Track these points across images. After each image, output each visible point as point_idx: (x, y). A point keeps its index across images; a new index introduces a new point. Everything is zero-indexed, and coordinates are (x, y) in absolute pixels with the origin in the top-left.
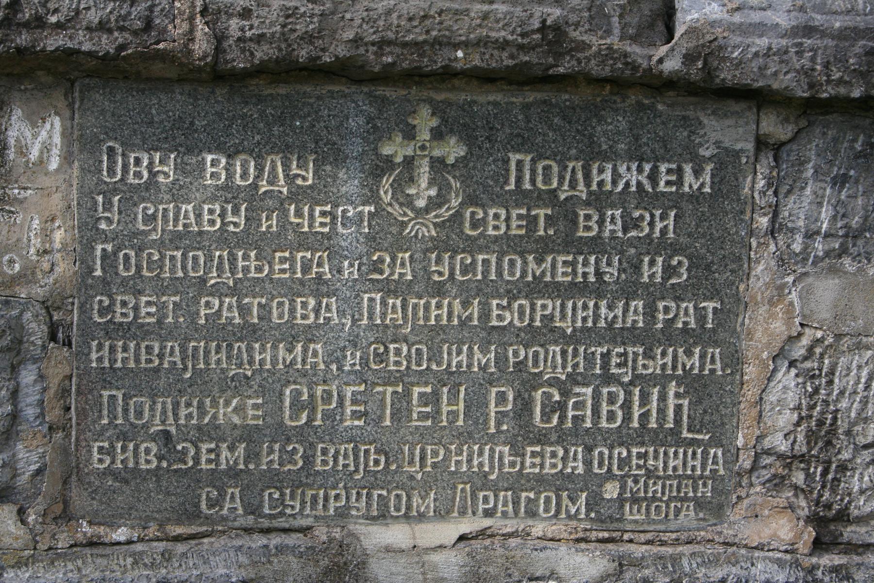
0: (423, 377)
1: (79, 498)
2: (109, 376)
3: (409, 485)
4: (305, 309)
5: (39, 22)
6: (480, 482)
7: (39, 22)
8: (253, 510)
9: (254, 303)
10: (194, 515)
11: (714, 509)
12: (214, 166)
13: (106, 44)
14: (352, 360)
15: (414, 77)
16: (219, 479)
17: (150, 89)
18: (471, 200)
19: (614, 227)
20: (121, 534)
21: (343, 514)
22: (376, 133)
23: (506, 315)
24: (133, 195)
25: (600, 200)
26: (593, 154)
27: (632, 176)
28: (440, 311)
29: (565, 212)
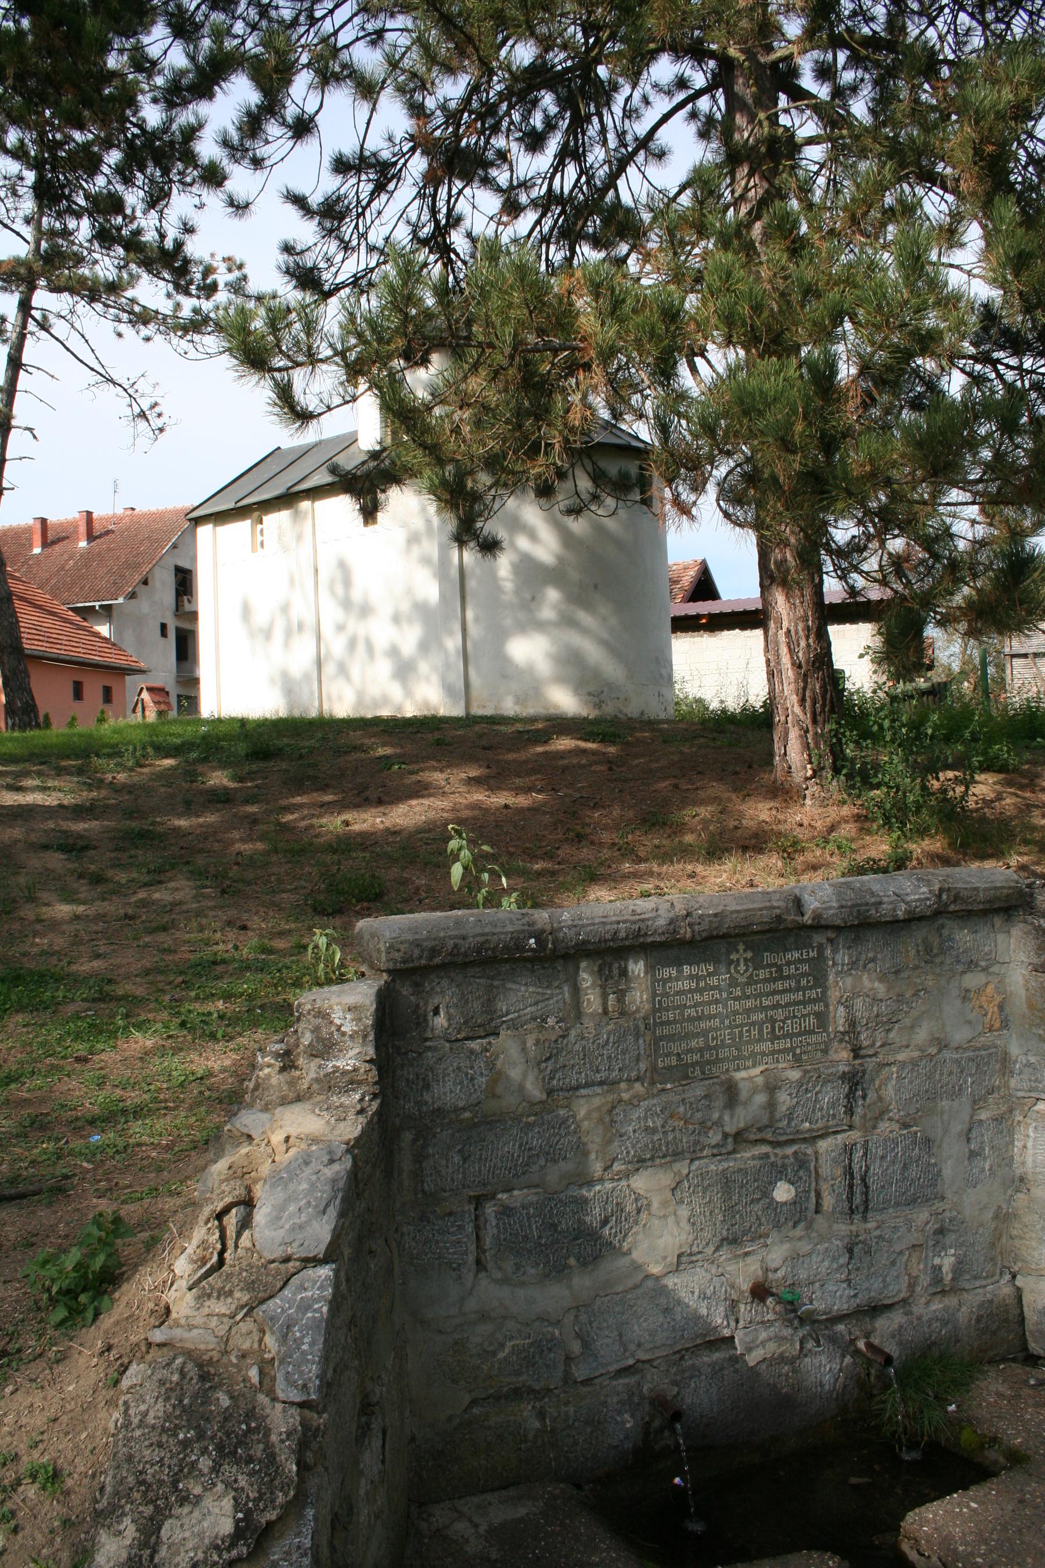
0: (746, 1025)
1: (656, 1077)
2: (662, 1038)
3: (745, 1058)
4: (713, 1009)
5: (646, 934)
6: (763, 1054)
7: (646, 934)
8: (703, 1073)
9: (699, 1009)
10: (687, 1077)
11: (825, 1052)
12: (686, 969)
13: (663, 938)
14: (727, 1022)
15: (737, 935)
16: (693, 1065)
17: (606, 941)
18: (755, 969)
19: (793, 971)
20: (669, 1086)
21: (727, 1070)
22: (728, 953)
23: (766, 1003)
24: (665, 981)
25: (789, 963)
26: (786, 950)
27: (796, 955)
28: (749, 1003)
29: (780, 969)
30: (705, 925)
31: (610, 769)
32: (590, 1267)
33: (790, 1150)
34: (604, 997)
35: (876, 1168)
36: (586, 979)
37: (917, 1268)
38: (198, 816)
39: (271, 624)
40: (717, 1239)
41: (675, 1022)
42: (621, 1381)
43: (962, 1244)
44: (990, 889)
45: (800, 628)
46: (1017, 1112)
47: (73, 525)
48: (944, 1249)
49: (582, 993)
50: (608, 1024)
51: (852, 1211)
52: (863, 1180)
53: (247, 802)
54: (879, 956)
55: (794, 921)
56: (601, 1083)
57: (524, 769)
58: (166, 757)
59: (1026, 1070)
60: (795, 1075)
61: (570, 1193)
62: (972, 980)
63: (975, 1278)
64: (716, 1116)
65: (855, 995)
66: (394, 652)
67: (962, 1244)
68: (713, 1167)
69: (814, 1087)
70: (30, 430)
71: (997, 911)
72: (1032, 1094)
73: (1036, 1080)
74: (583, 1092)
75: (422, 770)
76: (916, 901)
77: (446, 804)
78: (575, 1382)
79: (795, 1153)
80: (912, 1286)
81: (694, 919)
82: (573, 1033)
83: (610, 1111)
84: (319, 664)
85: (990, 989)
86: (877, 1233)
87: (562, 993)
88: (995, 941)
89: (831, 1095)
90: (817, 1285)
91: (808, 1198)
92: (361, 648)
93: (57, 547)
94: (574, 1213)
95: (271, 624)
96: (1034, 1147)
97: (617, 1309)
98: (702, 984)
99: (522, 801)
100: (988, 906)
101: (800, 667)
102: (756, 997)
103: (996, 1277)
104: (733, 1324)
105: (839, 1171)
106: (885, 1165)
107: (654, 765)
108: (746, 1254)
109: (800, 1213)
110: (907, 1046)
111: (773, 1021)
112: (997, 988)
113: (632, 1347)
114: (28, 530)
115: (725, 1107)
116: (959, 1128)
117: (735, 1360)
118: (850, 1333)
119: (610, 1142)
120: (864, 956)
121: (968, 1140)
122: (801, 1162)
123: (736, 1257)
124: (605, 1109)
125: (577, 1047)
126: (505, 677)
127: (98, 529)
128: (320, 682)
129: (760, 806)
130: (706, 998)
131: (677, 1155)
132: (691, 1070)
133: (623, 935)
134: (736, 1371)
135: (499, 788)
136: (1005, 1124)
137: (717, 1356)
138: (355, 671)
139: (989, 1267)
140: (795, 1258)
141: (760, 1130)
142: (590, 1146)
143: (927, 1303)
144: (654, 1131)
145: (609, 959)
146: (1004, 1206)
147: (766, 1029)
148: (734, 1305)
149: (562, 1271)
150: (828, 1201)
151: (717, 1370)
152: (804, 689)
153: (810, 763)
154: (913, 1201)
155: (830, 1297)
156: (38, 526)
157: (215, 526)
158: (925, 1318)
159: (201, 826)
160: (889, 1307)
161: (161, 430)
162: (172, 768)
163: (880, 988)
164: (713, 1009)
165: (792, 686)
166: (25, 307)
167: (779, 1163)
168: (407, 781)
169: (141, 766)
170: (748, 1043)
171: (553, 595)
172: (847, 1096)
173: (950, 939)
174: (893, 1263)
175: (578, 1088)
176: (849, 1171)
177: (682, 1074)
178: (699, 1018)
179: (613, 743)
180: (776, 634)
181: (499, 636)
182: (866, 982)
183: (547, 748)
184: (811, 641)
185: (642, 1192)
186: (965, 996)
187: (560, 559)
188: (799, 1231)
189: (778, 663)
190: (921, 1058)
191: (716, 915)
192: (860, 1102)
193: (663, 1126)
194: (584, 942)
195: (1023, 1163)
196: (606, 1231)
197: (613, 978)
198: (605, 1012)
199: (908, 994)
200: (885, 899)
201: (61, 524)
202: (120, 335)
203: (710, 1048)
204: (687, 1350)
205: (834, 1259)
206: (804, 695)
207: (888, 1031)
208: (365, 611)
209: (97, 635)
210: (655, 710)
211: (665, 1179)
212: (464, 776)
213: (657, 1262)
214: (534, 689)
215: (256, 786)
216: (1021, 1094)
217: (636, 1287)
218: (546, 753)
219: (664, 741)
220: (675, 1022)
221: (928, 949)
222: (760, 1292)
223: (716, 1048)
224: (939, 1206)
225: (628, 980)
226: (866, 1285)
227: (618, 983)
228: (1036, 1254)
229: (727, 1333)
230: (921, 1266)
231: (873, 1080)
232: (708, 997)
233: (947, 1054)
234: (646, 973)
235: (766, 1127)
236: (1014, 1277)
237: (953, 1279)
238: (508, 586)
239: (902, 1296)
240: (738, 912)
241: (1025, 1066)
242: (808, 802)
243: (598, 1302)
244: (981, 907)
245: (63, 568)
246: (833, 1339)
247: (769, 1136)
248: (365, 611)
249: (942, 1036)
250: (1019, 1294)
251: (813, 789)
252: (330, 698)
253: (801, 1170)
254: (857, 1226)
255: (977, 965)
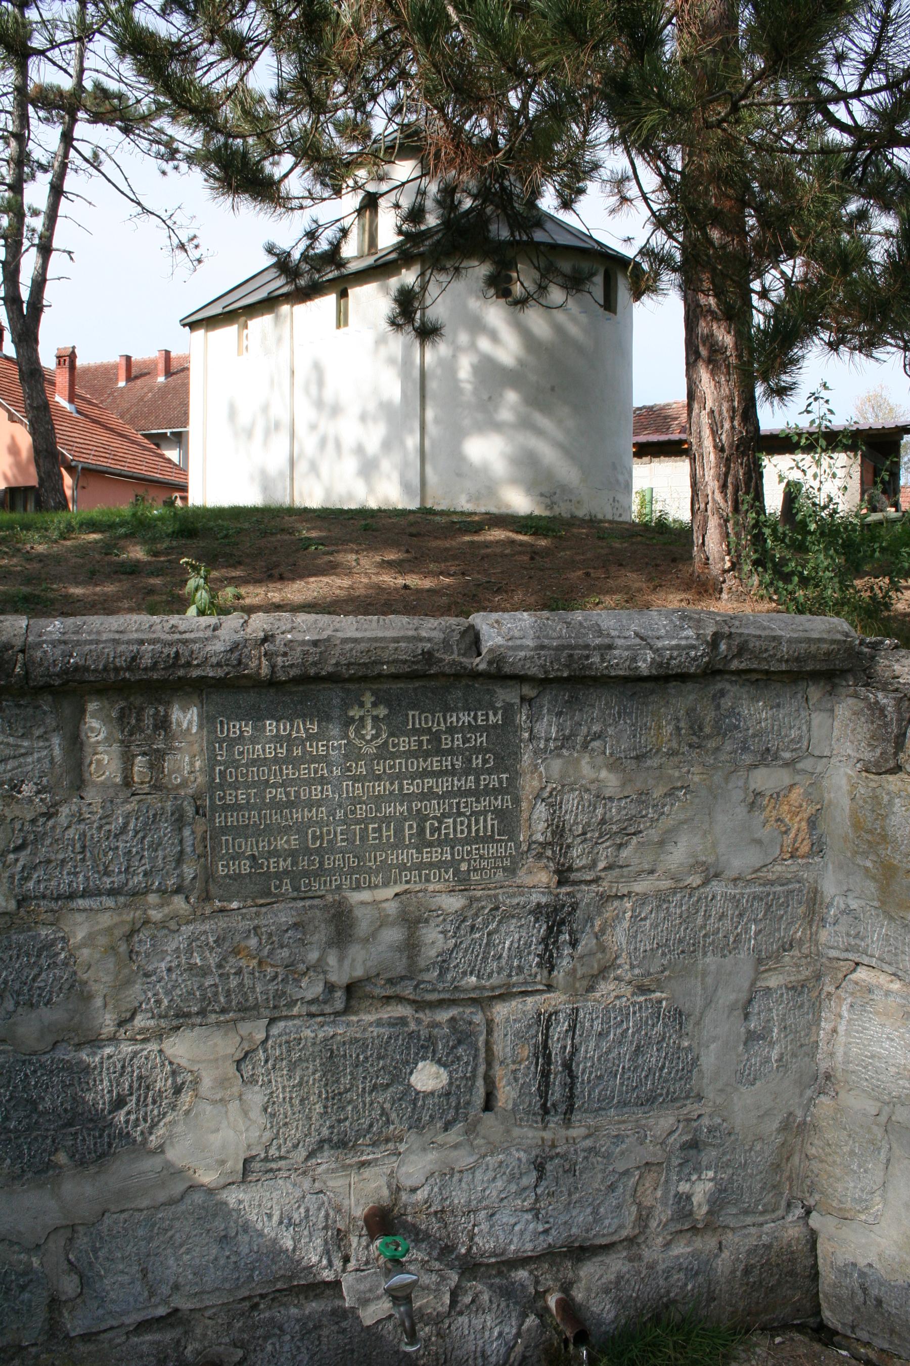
1: (213, 890)
2: (225, 830)
3: (370, 871)
4: (316, 792)
5: (188, 664)
6: (403, 867)
7: (188, 664)
10: (268, 894)
11: (511, 871)
12: (270, 726)
13: (220, 673)
14: (339, 814)
15: (364, 679)
17: (117, 670)
18: (392, 734)
19: (458, 743)
20: (235, 905)
21: (339, 888)
23: (410, 788)
24: (232, 742)
25: (451, 730)
26: (447, 709)
27: (465, 718)
28: (380, 788)
29: (436, 738)
30: (296, 656)
31: (532, 559)
32: (93, 1169)
33: (443, 1016)
34: (128, 760)
35: (589, 1050)
36: (97, 728)
37: (652, 1195)
38: (96, 585)
39: (253, 424)
40: (314, 1139)
41: (248, 806)
42: (148, 1337)
43: (727, 1165)
44: (799, 641)
45: (724, 409)
46: (827, 980)
47: (154, 363)
48: (698, 1169)
49: (88, 750)
50: (126, 801)
51: (546, 1111)
52: (568, 1066)
53: (152, 574)
54: (610, 731)
55: (453, 663)
56: (113, 892)
57: (443, 556)
58: (93, 532)
59: (844, 919)
60: (454, 903)
61: (59, 1054)
62: (766, 779)
63: (746, 1212)
64: (313, 956)
65: (565, 787)
66: (360, 450)
67: (727, 1165)
68: (308, 1033)
69: (486, 923)
70: (70, 253)
71: (815, 676)
72: (850, 956)
73: (857, 936)
74: (81, 903)
75: (338, 552)
76: (672, 648)
77: (346, 582)
78: (67, 1336)
79: (453, 1019)
80: (643, 1220)
81: (278, 645)
82: (64, 810)
83: (129, 936)
84: (292, 463)
85: (796, 795)
86: (588, 1143)
87: (50, 748)
88: (809, 723)
89: (517, 937)
90: (483, 1214)
91: (470, 1089)
92: (331, 446)
93: (139, 382)
94: (65, 1086)
95: (253, 424)
96: (848, 1033)
97: (141, 1232)
98: (297, 752)
99: (428, 583)
100: (795, 667)
101: (722, 450)
102: (392, 779)
103: (780, 1212)
104: (338, 1264)
105: (526, 1052)
106: (605, 1046)
107: (578, 558)
108: (363, 1164)
109: (450, 1109)
110: (652, 872)
111: (422, 818)
112: (807, 794)
113: (165, 1290)
114: (116, 367)
115: (330, 944)
116: (732, 997)
117: (340, 1314)
118: (537, 1282)
119: (128, 982)
120: (584, 729)
121: (747, 1016)
122: (462, 1035)
123: (345, 1167)
124: (118, 933)
125: (71, 833)
126: (459, 475)
127: (174, 366)
128: (292, 479)
129: (671, 597)
130: (303, 773)
131: (247, 1011)
132: (274, 882)
133: (146, 661)
134: (343, 1331)
135: (413, 572)
136: (808, 994)
137: (314, 1306)
138: (324, 469)
139: (768, 1198)
140: (446, 1174)
141: (391, 981)
142: (94, 987)
143: (667, 1245)
144: (204, 972)
145: (138, 701)
146: (799, 1113)
147: (409, 830)
148: (340, 1237)
149: (45, 1171)
150: (506, 1095)
151: (309, 1329)
152: (726, 475)
153: (729, 554)
154: (650, 1100)
155: (506, 1229)
156: (124, 362)
157: (207, 331)
158: (661, 1267)
159: (95, 594)
160: (607, 1248)
161: (199, 261)
162: (96, 542)
163: (610, 780)
164: (316, 792)
165: (712, 471)
166: (67, 138)
167: (424, 1033)
168: (319, 561)
169: (65, 539)
170: (375, 848)
171: (512, 397)
172: (544, 940)
173: (732, 712)
174: (612, 1188)
175: (71, 896)
176: (544, 1052)
177: (262, 888)
178: (290, 804)
179: (546, 536)
180: (699, 415)
181: (458, 434)
182: (586, 769)
183: (476, 538)
184: (736, 423)
185: (184, 1062)
186: (754, 801)
187: (521, 362)
188: (454, 1135)
189: (700, 446)
190: (674, 891)
191: (315, 643)
192: (566, 951)
193: (220, 966)
194: (77, 668)
195: (832, 1055)
196: (121, 1116)
197: (143, 731)
198: (127, 782)
199: (657, 793)
200: (619, 642)
201: (144, 362)
202: (164, 173)
203: (308, 852)
204: (262, 1296)
205: (512, 1178)
206: (726, 481)
207: (620, 846)
208: (336, 411)
209: (169, 461)
210: (604, 511)
211: (226, 1045)
212: (378, 559)
213: (208, 1168)
214: (491, 489)
215: (168, 561)
216: (833, 953)
217: (173, 1202)
218: (472, 542)
219: (599, 538)
220: (248, 806)
221: (696, 728)
222: (382, 1222)
223: (319, 851)
224: (692, 1108)
225: (169, 736)
226: (563, 1218)
227: (151, 739)
228: (839, 1187)
229: (327, 1275)
230: (659, 1193)
231: (590, 919)
232: (330, 776)
233: (717, 887)
234: (201, 727)
235: (402, 978)
236: (808, 1212)
237: (710, 1212)
238: (468, 387)
239: (624, 1233)
240: (355, 640)
241: (843, 912)
242: (725, 596)
243: (107, 1220)
244: (784, 667)
245: (142, 399)
246: (507, 1292)
247: (408, 991)
248: (336, 411)
249: (711, 860)
250: (813, 1238)
251: (731, 581)
252: (301, 494)
253: (461, 1045)
254: (554, 1131)
255: (776, 757)
